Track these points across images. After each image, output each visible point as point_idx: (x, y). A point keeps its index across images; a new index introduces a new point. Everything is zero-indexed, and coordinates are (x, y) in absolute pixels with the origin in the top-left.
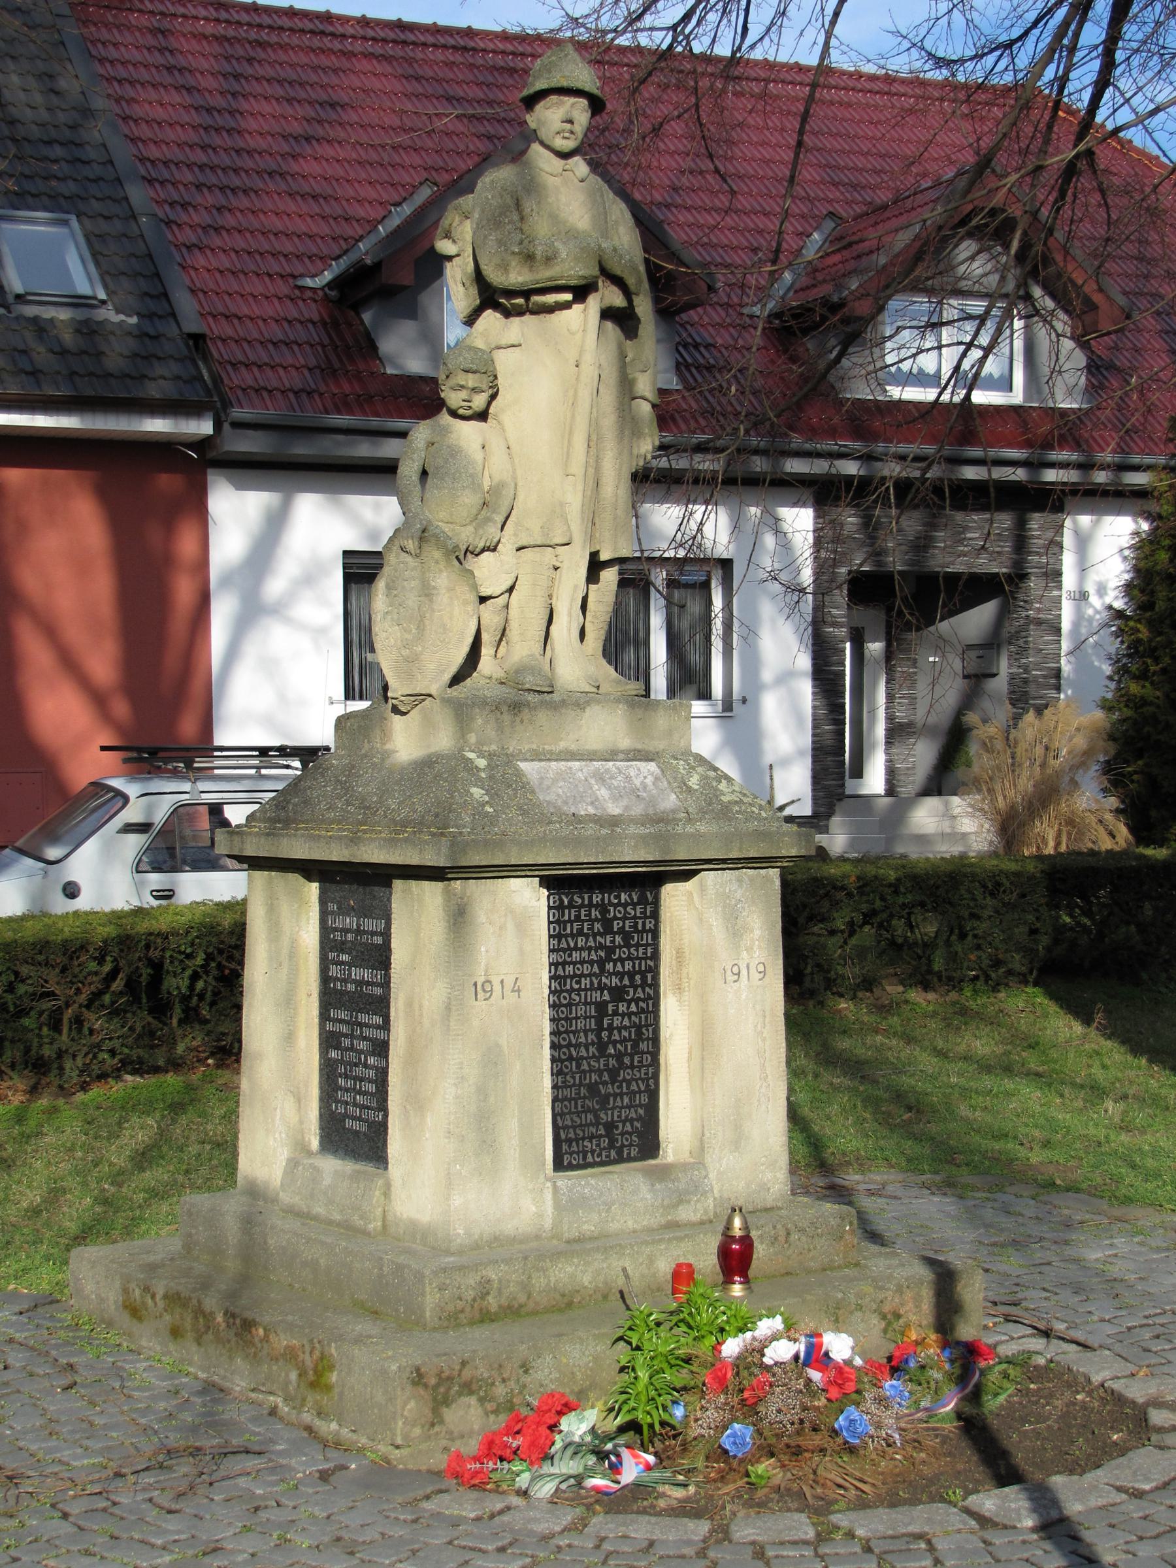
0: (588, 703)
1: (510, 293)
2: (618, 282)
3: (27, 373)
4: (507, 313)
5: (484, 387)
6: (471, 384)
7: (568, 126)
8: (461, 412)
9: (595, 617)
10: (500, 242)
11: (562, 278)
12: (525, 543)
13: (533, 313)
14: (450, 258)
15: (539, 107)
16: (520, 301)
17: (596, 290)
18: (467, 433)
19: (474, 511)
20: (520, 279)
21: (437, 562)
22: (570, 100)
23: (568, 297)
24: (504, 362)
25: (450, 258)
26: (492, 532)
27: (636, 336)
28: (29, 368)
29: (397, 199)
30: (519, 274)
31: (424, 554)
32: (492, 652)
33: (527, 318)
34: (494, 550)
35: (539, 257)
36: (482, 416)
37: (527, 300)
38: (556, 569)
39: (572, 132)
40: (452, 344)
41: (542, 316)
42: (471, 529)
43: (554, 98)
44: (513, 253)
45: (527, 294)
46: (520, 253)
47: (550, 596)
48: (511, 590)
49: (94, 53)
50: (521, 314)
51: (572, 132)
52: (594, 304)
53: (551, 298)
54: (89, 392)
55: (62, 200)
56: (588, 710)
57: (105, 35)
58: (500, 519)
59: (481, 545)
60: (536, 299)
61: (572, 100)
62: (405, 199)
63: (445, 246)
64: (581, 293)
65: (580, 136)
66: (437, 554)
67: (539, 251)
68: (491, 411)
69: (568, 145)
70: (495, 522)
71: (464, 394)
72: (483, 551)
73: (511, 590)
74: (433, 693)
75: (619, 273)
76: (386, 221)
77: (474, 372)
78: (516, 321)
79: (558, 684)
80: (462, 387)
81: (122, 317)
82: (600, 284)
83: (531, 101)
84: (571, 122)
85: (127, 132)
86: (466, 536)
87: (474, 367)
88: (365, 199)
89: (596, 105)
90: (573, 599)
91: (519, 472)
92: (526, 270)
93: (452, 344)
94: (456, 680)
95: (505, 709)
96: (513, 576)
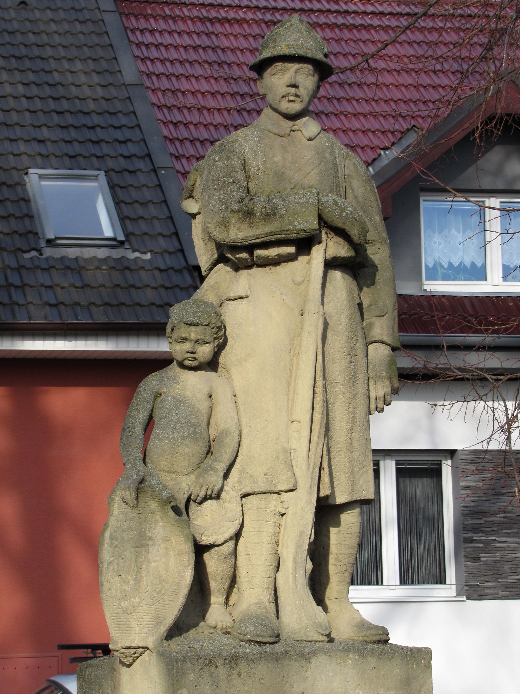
0: (314, 653)
1: (235, 248)
2: (341, 233)
3: (51, 305)
4: (237, 267)
5: (208, 338)
6: (193, 336)
7: (293, 90)
8: (187, 363)
9: (337, 559)
10: (222, 201)
11: (281, 232)
12: (248, 490)
13: (259, 266)
14: (193, 216)
15: (267, 74)
16: (244, 255)
17: (320, 242)
18: (191, 385)
19: (196, 460)
20: (240, 235)
21: (153, 513)
22: (293, 67)
23: (291, 249)
24: (234, 315)
25: (193, 216)
26: (215, 480)
27: (373, 283)
28: (53, 301)
29: (387, 144)
30: (239, 230)
31: (141, 505)
32: (222, 599)
33: (255, 270)
34: (218, 497)
35: (258, 214)
36: (212, 365)
37: (251, 254)
38: (283, 515)
39: (297, 96)
40: (431, 265)
41: (268, 268)
42: (192, 477)
43: (279, 65)
44: (233, 211)
45: (250, 248)
46: (239, 211)
47: (277, 543)
48: (237, 536)
49: (132, 38)
50: (249, 267)
51: (297, 96)
52: (318, 255)
53: (273, 252)
54: (103, 319)
55: (94, 159)
56: (313, 661)
57: (143, 24)
58: (222, 467)
59: (202, 494)
60: (258, 252)
61: (296, 66)
62: (393, 144)
63: (191, 206)
64: (305, 244)
65: (306, 99)
66: (153, 505)
67: (258, 208)
68: (221, 360)
69: (296, 107)
70: (216, 471)
71: (187, 346)
72: (205, 499)
73: (237, 536)
74: (150, 645)
75: (340, 225)
76: (376, 163)
77: (197, 325)
78: (244, 273)
79: (284, 635)
80: (186, 339)
81: (137, 254)
82: (323, 235)
83: (261, 67)
84: (295, 86)
85: (155, 101)
86: (185, 485)
87: (196, 321)
88: (358, 145)
89: (323, 70)
90: (299, 546)
91: (244, 421)
92: (246, 226)
93: (431, 265)
94: (177, 630)
95: (220, 662)
96: (239, 522)
